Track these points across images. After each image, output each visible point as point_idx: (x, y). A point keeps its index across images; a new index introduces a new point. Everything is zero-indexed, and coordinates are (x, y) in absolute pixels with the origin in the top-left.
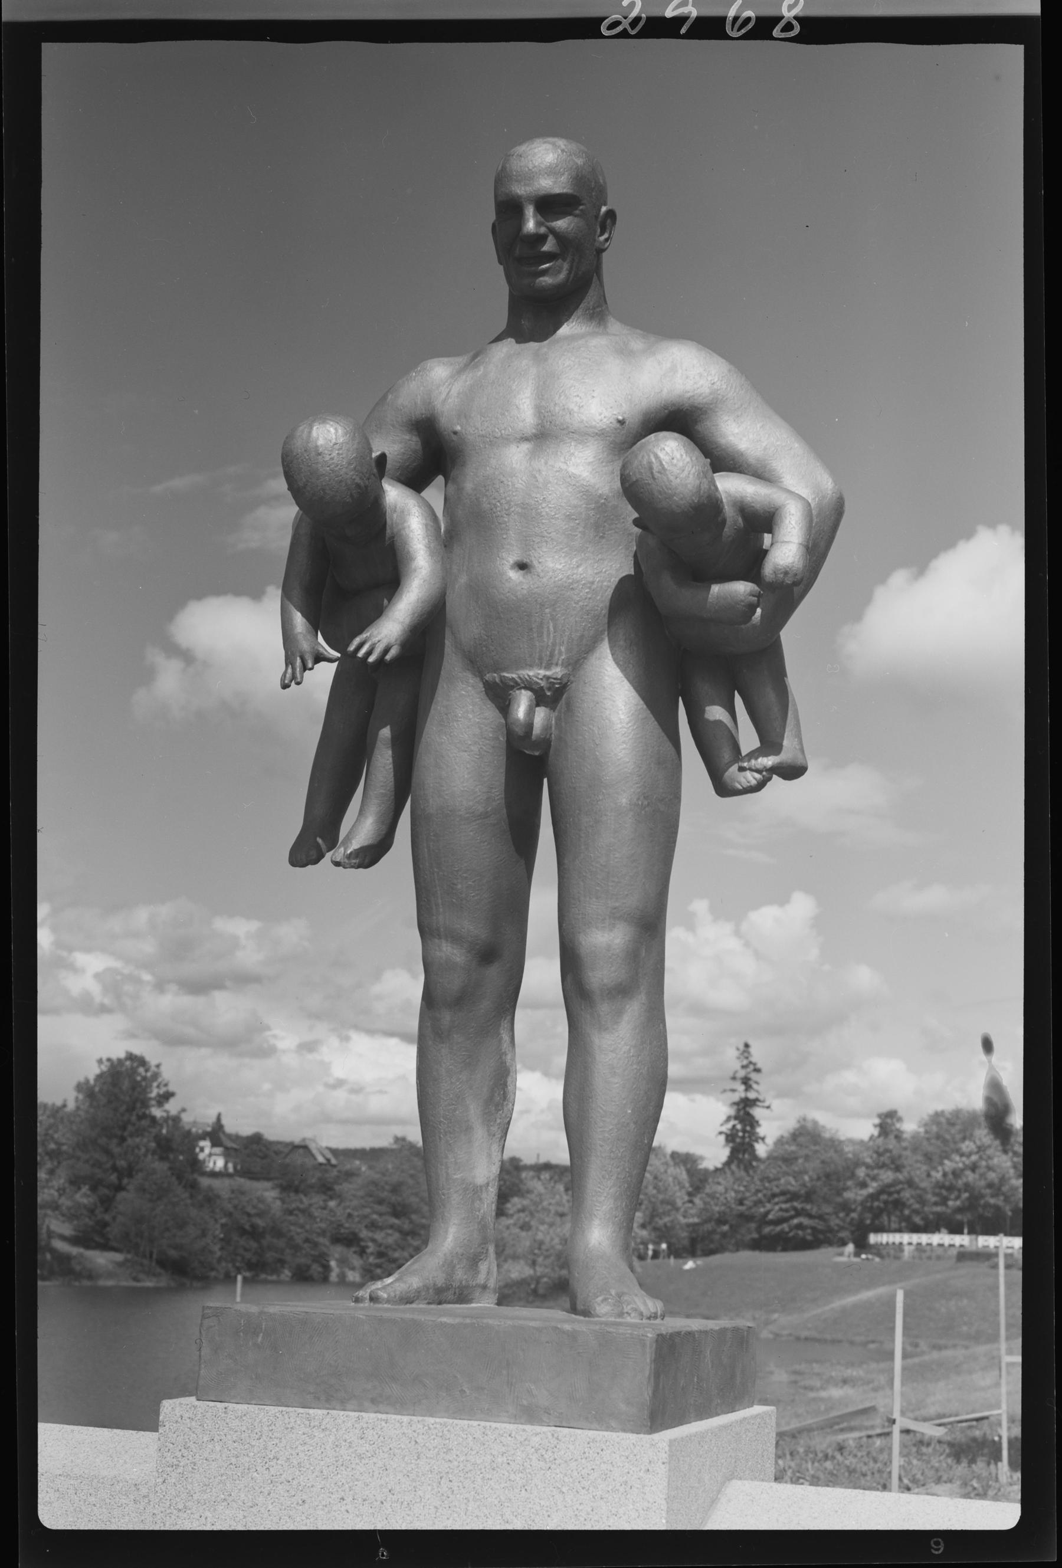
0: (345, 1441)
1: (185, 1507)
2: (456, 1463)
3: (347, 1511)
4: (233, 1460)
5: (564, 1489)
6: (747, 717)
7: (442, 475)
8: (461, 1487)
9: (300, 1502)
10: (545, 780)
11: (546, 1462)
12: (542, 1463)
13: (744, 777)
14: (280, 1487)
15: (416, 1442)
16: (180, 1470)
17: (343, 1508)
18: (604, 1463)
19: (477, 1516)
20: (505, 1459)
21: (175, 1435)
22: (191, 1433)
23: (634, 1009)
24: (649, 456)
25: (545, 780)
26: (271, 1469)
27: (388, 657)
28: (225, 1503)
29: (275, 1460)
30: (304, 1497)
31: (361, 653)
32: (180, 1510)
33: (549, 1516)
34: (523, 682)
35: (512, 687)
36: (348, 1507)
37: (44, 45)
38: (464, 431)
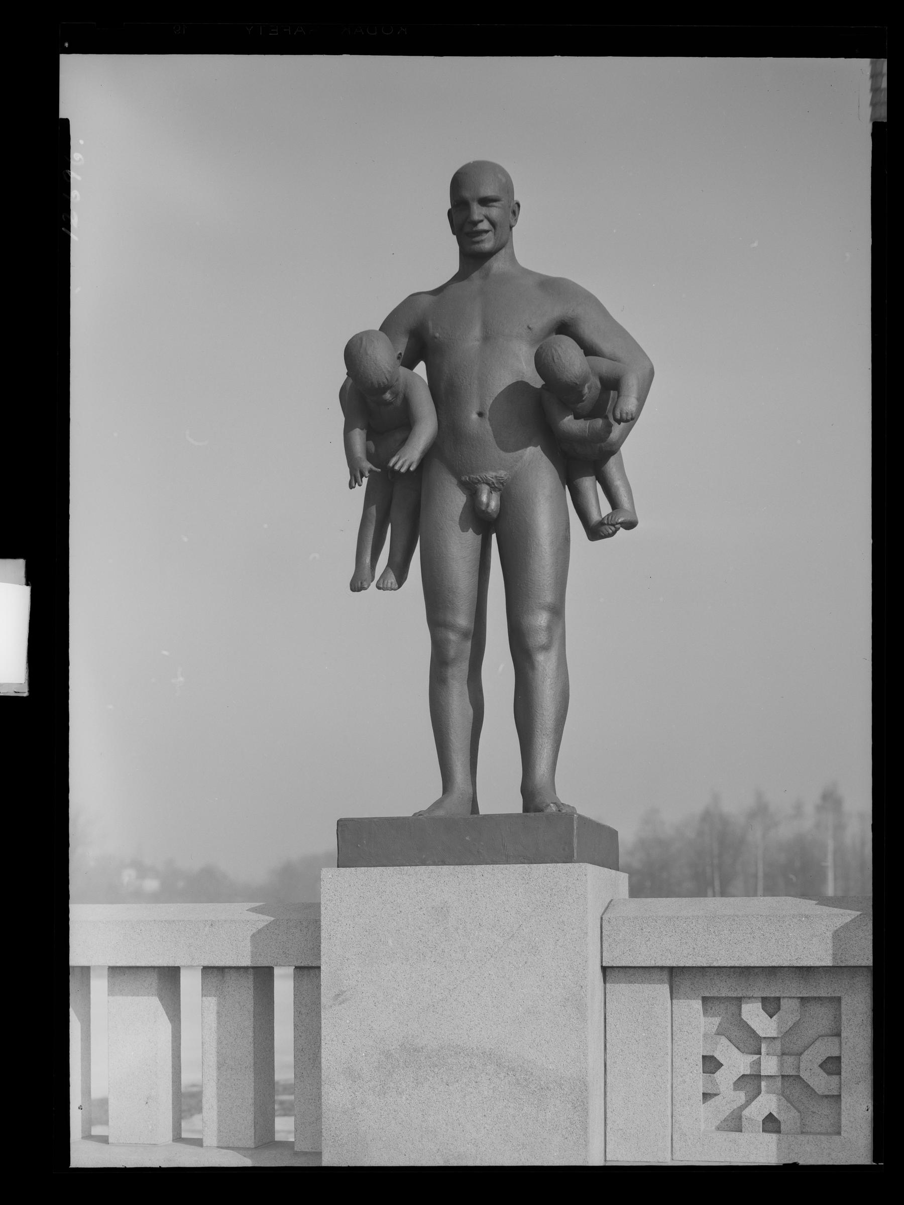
0: (421, 880)
1: (338, 920)
2: (479, 886)
3: (424, 914)
4: (362, 895)
5: (535, 892)
6: (496, 538)
7: (425, 362)
8: (482, 897)
9: (399, 912)
10: (494, 536)
11: (525, 880)
12: (524, 881)
13: (605, 529)
14: (388, 906)
15: (458, 877)
16: (334, 902)
17: (422, 913)
18: (555, 878)
19: (491, 910)
20: (504, 881)
21: (329, 885)
22: (338, 883)
23: (553, 654)
24: (551, 349)
25: (494, 536)
26: (382, 897)
27: (412, 469)
28: (359, 916)
29: (384, 893)
30: (401, 910)
31: (397, 468)
32: (335, 922)
33: (528, 906)
34: (483, 480)
35: (476, 483)
36: (425, 912)
37: (60, 55)
38: (441, 337)
